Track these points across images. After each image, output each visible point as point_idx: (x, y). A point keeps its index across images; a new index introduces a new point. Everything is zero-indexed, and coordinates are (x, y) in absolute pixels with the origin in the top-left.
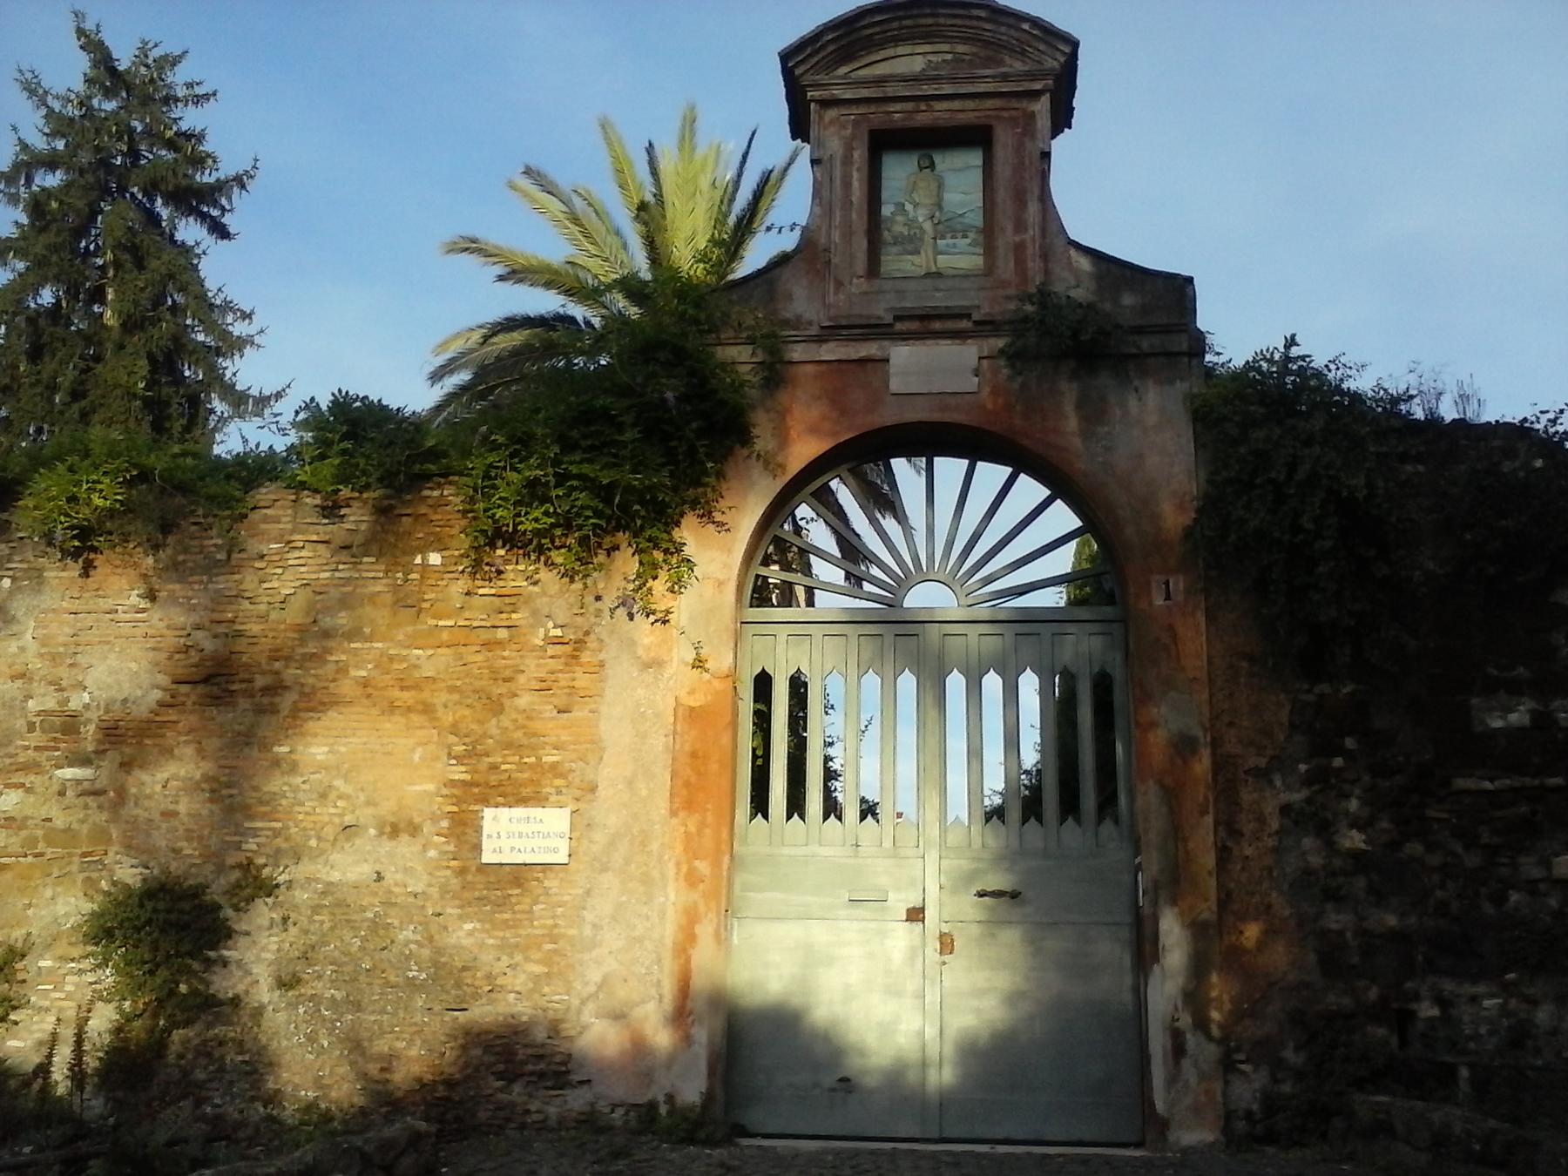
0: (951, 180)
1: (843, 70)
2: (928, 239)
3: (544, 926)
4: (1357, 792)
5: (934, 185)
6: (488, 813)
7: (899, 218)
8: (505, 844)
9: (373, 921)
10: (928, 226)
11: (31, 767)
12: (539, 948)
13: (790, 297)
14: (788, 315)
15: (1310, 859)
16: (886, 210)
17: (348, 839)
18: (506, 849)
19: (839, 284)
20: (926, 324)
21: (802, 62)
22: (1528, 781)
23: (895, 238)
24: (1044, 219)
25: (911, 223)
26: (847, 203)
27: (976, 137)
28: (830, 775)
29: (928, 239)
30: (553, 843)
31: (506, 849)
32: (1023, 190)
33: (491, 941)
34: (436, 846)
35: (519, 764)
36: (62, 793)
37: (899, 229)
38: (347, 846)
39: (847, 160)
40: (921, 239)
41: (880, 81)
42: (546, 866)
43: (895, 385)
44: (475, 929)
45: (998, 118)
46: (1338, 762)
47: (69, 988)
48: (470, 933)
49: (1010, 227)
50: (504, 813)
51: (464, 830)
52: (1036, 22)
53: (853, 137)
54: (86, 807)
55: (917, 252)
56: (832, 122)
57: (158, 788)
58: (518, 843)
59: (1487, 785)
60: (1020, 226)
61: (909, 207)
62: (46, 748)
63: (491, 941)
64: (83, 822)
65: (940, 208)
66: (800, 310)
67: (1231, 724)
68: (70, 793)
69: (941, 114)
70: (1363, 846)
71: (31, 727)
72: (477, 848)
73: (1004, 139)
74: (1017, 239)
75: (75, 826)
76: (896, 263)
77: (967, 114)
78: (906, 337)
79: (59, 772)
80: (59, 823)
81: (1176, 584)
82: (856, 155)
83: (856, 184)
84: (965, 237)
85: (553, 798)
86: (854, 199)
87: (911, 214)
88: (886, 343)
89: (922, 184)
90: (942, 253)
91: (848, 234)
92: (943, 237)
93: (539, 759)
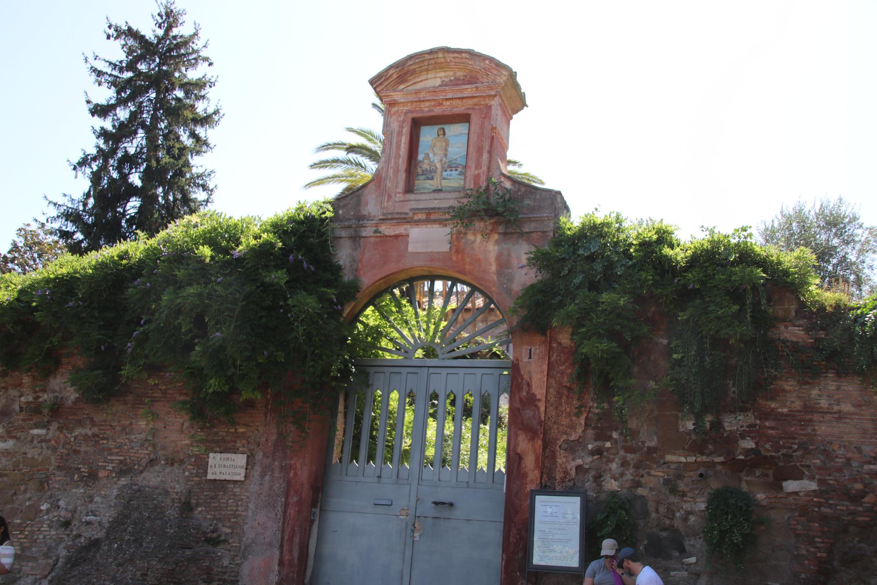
0: (452, 141)
1: (402, 87)
2: (439, 171)
3: (232, 510)
4: (617, 460)
5: (444, 144)
6: (211, 455)
7: (426, 161)
8: (218, 470)
9: (156, 505)
10: (439, 166)
11: (21, 429)
12: (229, 521)
13: (367, 204)
14: (365, 213)
15: (589, 493)
16: (420, 157)
17: (152, 466)
18: (218, 473)
19: (390, 197)
20: (430, 217)
21: (381, 84)
22: (704, 458)
23: (423, 171)
24: (490, 161)
25: (431, 163)
26: (398, 155)
27: (464, 118)
28: (373, 438)
29: (439, 171)
30: (238, 470)
31: (218, 473)
32: (493, 144)
33: (209, 516)
34: (189, 470)
35: (227, 432)
36: (32, 441)
37: (426, 166)
38: (151, 469)
39: (400, 134)
40: (435, 172)
41: (417, 92)
42: (235, 482)
43: (411, 248)
44: (202, 511)
45: (473, 109)
46: (608, 444)
47: (26, 533)
48: (201, 512)
49: (473, 168)
50: (218, 456)
51: (202, 464)
52: (492, 60)
53: (404, 121)
54: (42, 448)
55: (432, 179)
56: (395, 114)
57: (72, 439)
58: (223, 470)
59: (683, 459)
60: (478, 166)
61: (431, 155)
62: (28, 420)
63: (209, 516)
64: (39, 455)
65: (446, 155)
66: (371, 210)
67: (555, 423)
68: (35, 442)
69: (447, 108)
70: (617, 489)
71: (21, 409)
72: (206, 473)
73: (474, 119)
74: (476, 172)
75: (36, 457)
76: (421, 183)
77: (460, 108)
78: (417, 223)
79: (31, 431)
80: (90, 433)
81: (535, 351)
82: (404, 131)
83: (403, 145)
84: (456, 170)
85: (241, 449)
86: (401, 154)
87: (432, 159)
88: (408, 226)
89: (438, 144)
90: (444, 179)
91: (396, 172)
92: (446, 171)
93: (236, 430)
